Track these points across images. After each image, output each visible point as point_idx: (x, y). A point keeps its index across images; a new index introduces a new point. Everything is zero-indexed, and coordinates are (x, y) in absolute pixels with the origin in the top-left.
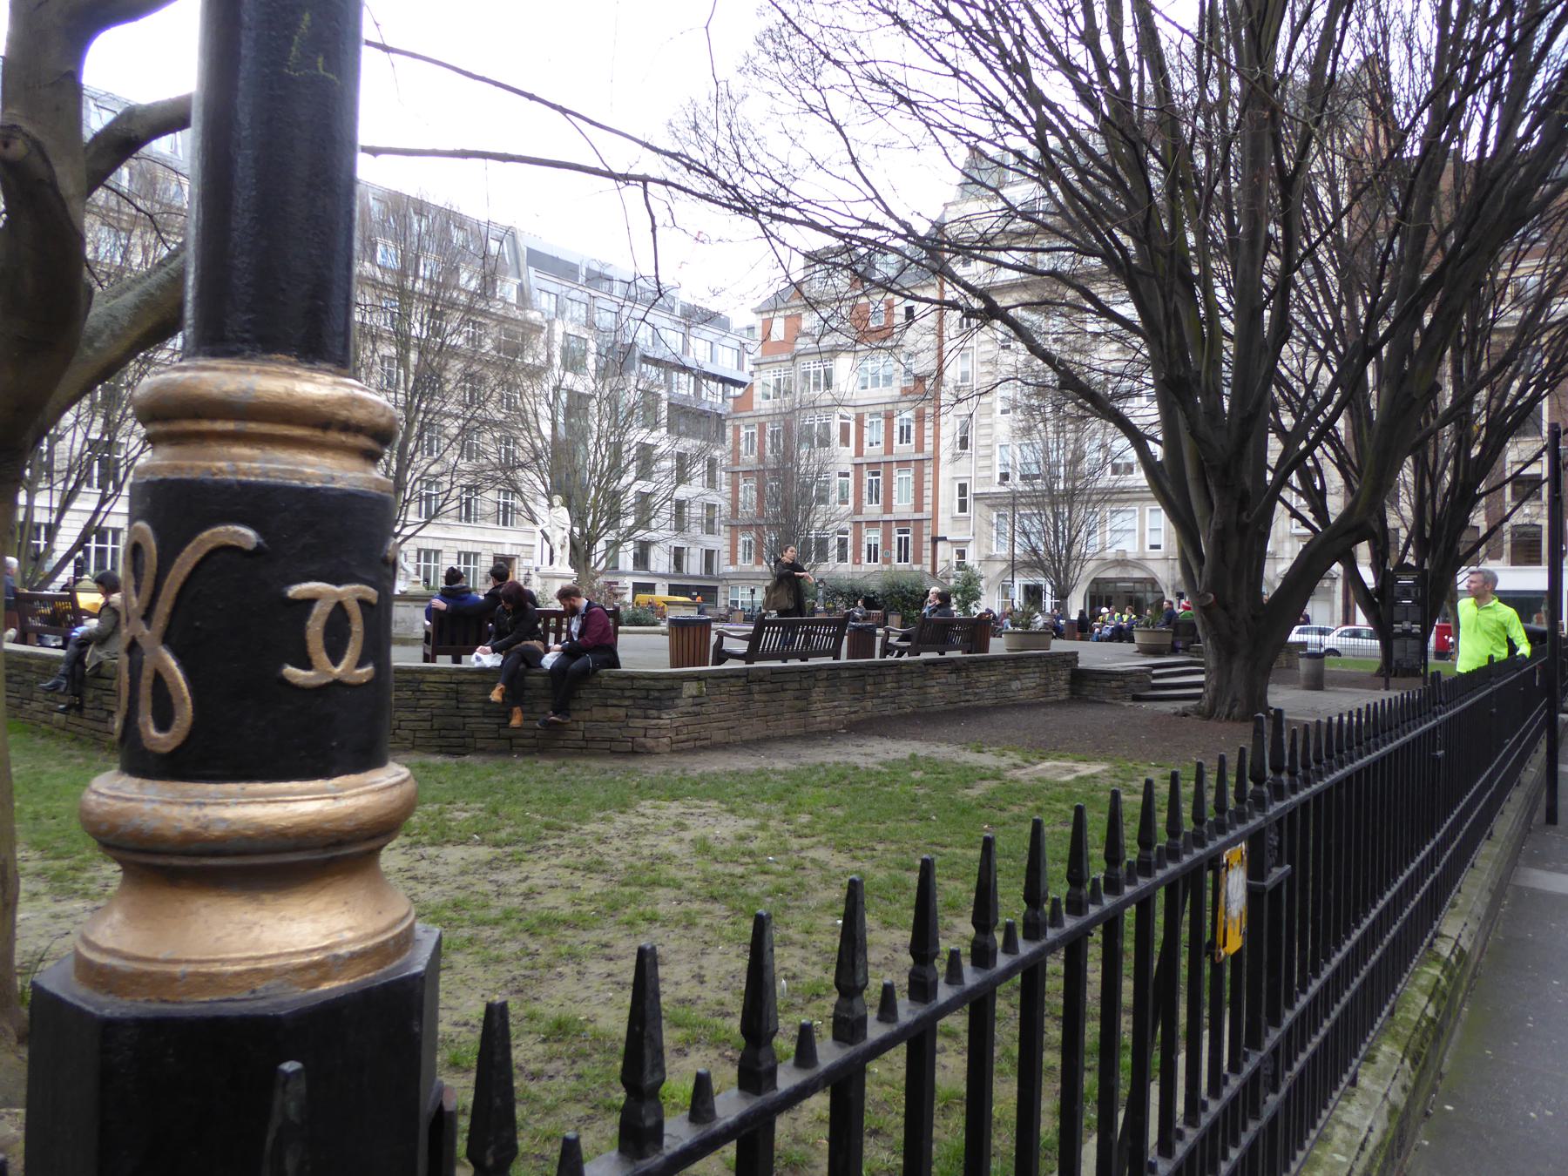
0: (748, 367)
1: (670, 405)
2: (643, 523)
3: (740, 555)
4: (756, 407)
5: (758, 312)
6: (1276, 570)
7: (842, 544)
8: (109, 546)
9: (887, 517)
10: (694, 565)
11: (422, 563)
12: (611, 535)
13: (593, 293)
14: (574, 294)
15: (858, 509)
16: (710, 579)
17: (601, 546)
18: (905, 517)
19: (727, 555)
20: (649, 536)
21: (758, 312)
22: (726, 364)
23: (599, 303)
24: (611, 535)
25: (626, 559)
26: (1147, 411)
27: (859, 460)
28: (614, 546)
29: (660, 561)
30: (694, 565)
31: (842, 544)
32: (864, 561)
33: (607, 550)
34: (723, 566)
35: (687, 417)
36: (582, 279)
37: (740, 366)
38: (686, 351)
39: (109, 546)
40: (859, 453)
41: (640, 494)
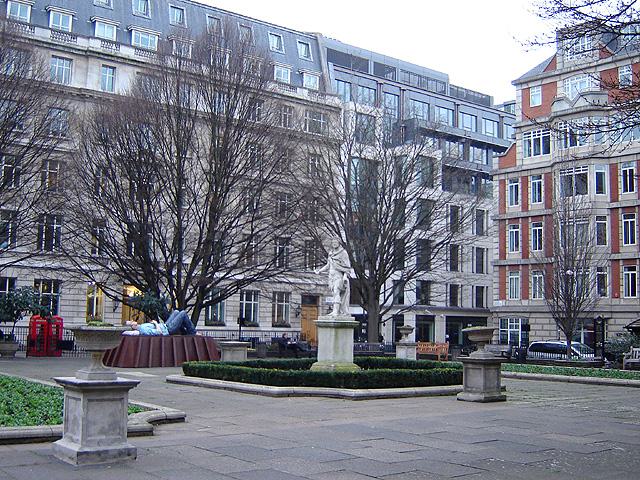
0: (509, 131)
1: (445, 169)
2: (424, 264)
3: (531, 291)
4: (519, 163)
5: (517, 83)
6: (187, 297)
7: (601, 280)
8: (253, 302)
9: (525, 214)
10: (467, 301)
11: (245, 302)
12: (397, 275)
13: (381, 81)
14: (364, 82)
15: (616, 249)
16: (481, 312)
17: (389, 283)
18: (631, 256)
19: (496, 291)
20: (427, 277)
21: (517, 83)
22: (488, 132)
23: (386, 88)
24: (397, 275)
25: (410, 297)
26: (66, 314)
27: (615, 205)
28: (400, 284)
29: (439, 298)
30: (467, 301)
31: (601, 280)
32: (623, 295)
33: (394, 288)
34: (494, 302)
35: (458, 177)
36: (371, 71)
37: (500, 134)
38: (455, 124)
39: (253, 302)
40: (614, 198)
41: (419, 241)
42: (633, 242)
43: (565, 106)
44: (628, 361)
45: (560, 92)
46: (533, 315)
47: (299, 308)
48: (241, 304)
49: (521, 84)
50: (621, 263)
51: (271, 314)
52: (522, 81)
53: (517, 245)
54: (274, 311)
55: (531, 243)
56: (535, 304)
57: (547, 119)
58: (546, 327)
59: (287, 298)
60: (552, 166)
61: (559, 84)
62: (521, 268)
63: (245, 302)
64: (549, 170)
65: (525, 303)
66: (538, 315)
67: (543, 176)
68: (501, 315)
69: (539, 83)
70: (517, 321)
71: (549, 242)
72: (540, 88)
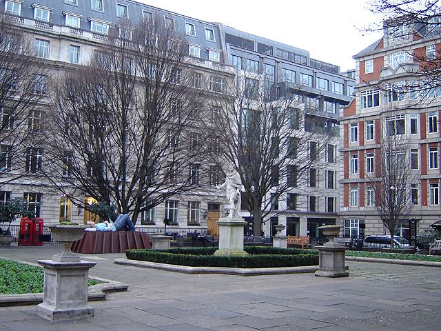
0: (351, 90)
1: (307, 116)
2: (292, 182)
3: (366, 201)
4: (357, 112)
5: (356, 57)
6: (129, 204)
7: (414, 193)
8: (174, 208)
9: (362, 148)
10: (322, 208)
11: (169, 208)
12: (274, 190)
13: (262, 56)
14: (251, 56)
15: (424, 172)
16: (331, 215)
17: (268, 195)
18: (435, 177)
19: (342, 201)
20: (294, 191)
21: (356, 57)
22: (337, 91)
23: (266, 61)
24: (274, 190)
25: (283, 205)
26: (46, 217)
27: (424, 141)
28: (276, 196)
29: (302, 205)
30: (322, 208)
31: (414, 193)
32: (429, 204)
33: (271, 198)
34: (340, 208)
35: (315, 122)
36: (256, 49)
37: (345, 93)
38: (314, 86)
39: (174, 208)
40: (423, 136)
41: (289, 166)
42: (436, 167)
43: (389, 73)
44: (433, 249)
45: (386, 64)
46: (367, 217)
47: (206, 212)
48: (166, 210)
49: (359, 58)
50: (428, 181)
51: (186, 217)
52: (360, 56)
53: (356, 169)
54: (188, 215)
55: (366, 168)
56: (369, 209)
57: (377, 82)
58: (376, 226)
59: (198, 205)
60: (380, 114)
61: (385, 58)
62: (359, 185)
63: (169, 208)
64: (378, 117)
65: (362, 209)
66: (371, 217)
67: (374, 121)
68: (345, 217)
69: (371, 57)
70: (356, 222)
71: (378, 167)
72: (372, 61)
